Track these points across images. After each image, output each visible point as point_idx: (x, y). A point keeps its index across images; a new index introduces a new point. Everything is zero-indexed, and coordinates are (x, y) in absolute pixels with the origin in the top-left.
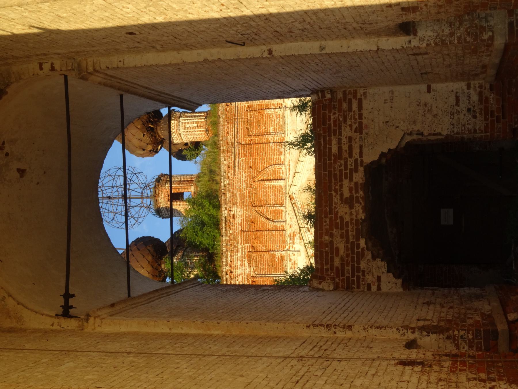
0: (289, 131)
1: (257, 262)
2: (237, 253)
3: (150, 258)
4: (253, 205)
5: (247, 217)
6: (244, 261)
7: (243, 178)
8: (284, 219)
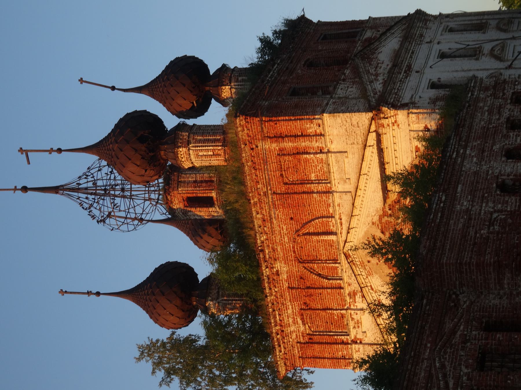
0: (336, 181)
1: (311, 319)
2: (287, 310)
3: (178, 302)
4: (301, 261)
5: (294, 273)
6: (297, 319)
7: (283, 230)
8: (340, 275)
